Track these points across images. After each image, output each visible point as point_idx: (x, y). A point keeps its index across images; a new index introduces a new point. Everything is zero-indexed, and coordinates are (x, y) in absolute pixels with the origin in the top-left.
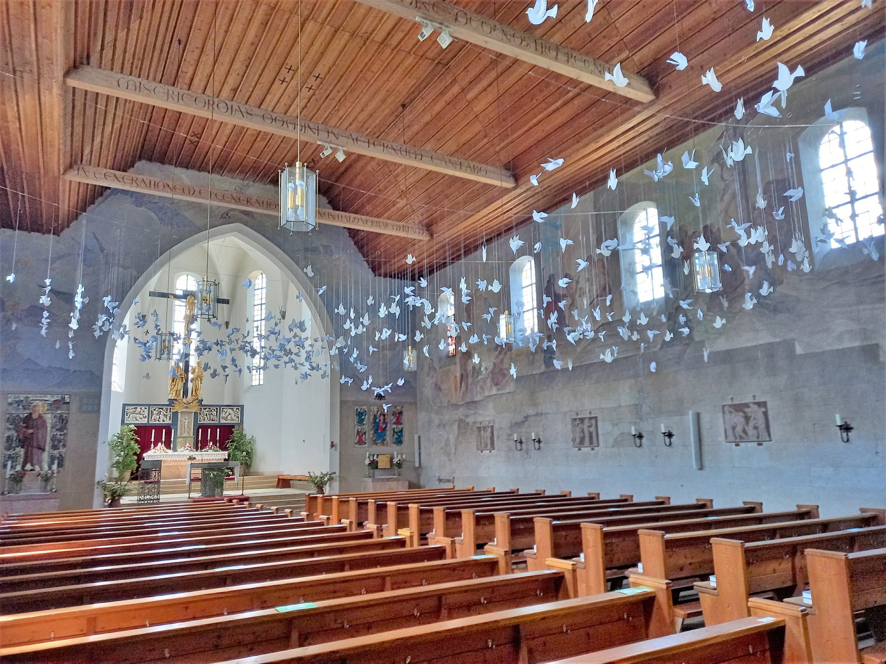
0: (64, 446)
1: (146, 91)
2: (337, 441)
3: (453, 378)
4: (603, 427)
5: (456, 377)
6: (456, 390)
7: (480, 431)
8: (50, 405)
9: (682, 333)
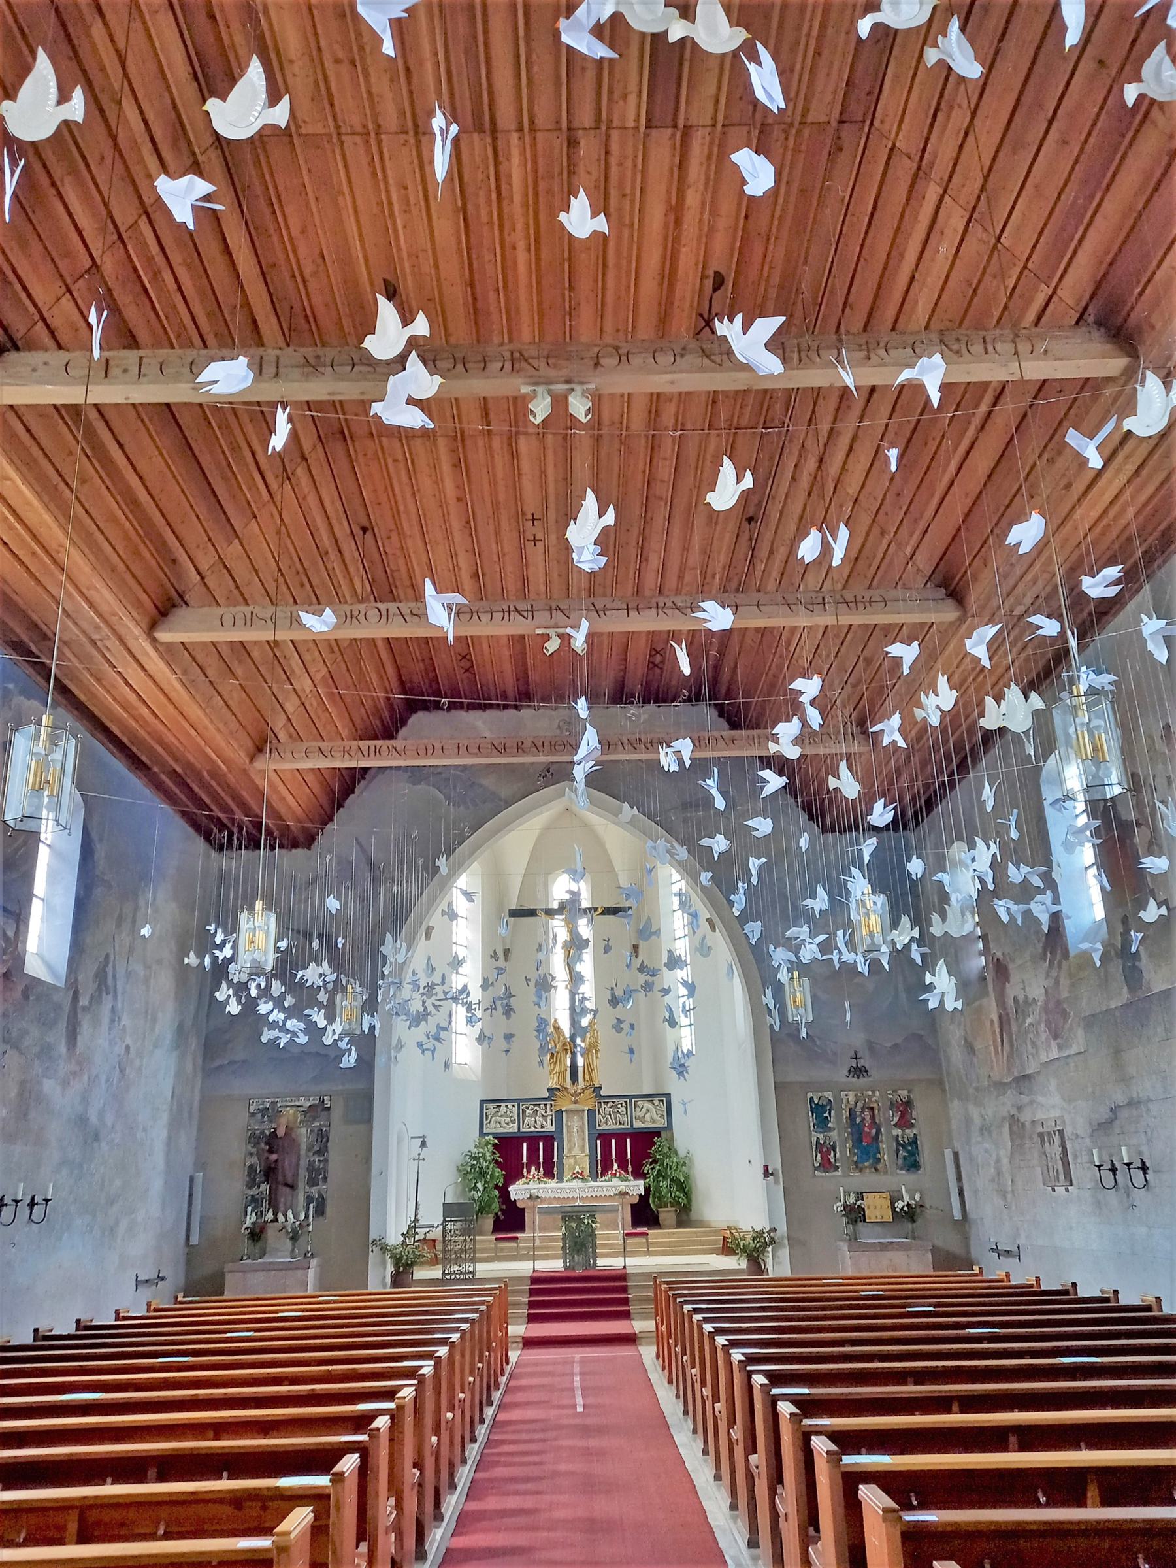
0: (325, 1179)
2: (776, 1164)
3: (988, 1024)
5: (992, 1021)
7: (1043, 1141)
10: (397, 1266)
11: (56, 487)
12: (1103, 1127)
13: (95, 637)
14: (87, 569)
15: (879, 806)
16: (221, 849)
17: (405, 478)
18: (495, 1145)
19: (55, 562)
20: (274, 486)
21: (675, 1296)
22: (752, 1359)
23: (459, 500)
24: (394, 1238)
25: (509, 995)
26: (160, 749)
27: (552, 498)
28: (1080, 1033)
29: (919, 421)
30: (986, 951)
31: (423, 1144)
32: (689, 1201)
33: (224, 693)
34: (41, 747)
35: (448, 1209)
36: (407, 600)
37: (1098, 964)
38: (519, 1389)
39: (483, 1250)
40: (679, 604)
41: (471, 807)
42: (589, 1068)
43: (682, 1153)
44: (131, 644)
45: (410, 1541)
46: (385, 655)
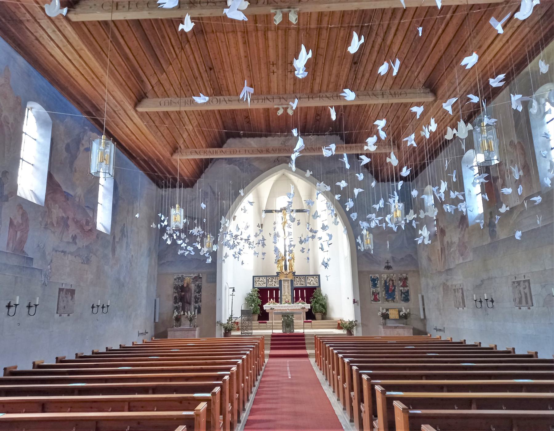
0: (201, 301)
1: (174, 104)
2: (358, 299)
4: (535, 289)
5: (438, 250)
6: (439, 261)
7: (455, 292)
8: (193, 279)
9: (535, 201)
10: (225, 330)
11: (100, 53)
12: (478, 287)
13: (115, 109)
14: (112, 84)
15: (405, 169)
16: (162, 187)
17: (225, 49)
18: (258, 291)
19: (100, 81)
20: (178, 52)
21: (323, 342)
22: (351, 362)
23: (245, 57)
24: (224, 321)
25: (264, 240)
26: (139, 151)
27: (280, 55)
28: (471, 254)
29: (423, 20)
30: (437, 225)
31: (234, 290)
32: (326, 311)
33: (161, 131)
34: (102, 147)
35: (243, 312)
36: (226, 95)
37: (482, 227)
38: (268, 371)
39: (255, 326)
40: (328, 96)
41: (250, 174)
42: (291, 266)
43: (324, 295)
44: (128, 112)
45: (236, 417)
46: (218, 117)
